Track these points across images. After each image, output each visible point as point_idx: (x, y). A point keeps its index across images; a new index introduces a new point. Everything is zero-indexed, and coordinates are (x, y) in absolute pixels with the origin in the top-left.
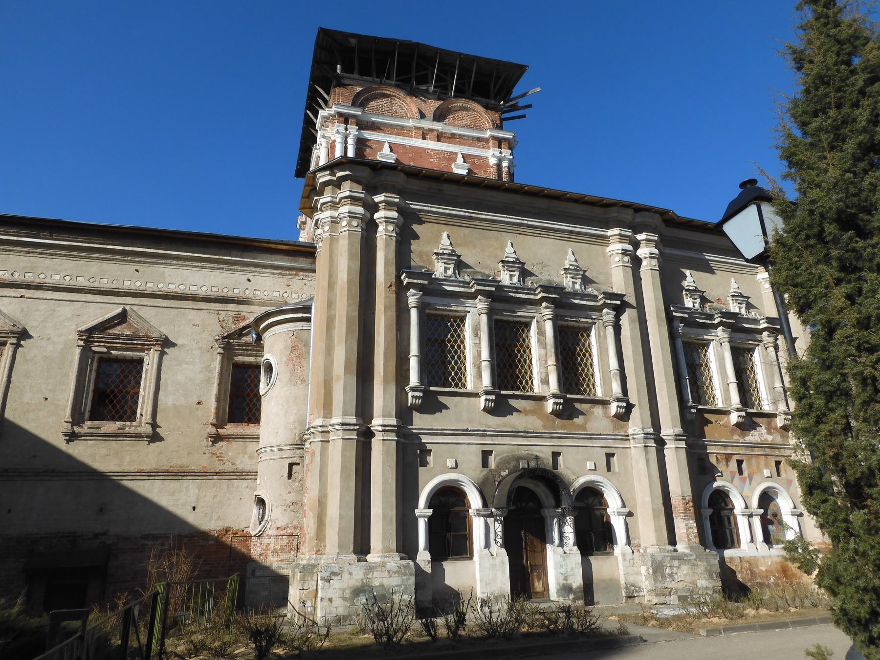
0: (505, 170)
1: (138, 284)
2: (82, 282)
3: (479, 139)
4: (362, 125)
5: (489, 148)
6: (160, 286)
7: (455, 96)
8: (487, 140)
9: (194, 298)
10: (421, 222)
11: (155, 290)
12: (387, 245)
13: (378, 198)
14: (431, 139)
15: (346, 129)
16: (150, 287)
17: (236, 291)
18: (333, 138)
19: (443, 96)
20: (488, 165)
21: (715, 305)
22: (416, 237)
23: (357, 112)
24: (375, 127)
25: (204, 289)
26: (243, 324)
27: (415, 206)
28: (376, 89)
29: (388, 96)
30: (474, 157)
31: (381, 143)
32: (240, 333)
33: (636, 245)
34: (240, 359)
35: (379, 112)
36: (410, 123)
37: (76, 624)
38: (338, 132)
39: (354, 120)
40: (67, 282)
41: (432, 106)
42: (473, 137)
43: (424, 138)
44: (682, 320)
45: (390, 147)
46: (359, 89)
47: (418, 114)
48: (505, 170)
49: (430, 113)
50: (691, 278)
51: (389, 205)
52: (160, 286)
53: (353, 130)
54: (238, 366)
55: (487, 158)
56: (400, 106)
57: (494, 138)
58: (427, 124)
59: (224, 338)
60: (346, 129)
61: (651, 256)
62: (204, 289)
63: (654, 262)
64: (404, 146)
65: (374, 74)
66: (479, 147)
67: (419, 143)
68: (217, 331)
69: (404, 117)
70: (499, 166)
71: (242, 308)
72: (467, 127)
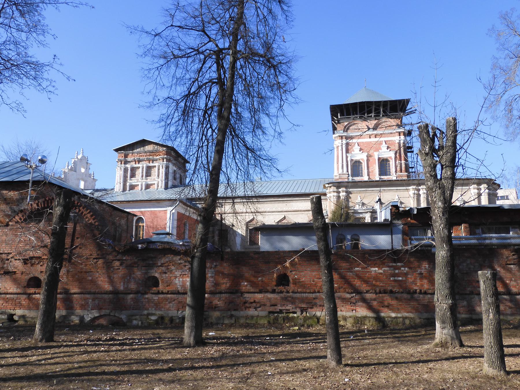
2: (274, 210)
3: (391, 133)
4: (347, 138)
7: (383, 116)
10: (351, 193)
13: (340, 190)
16: (290, 209)
19: (377, 118)
20: (395, 143)
22: (350, 198)
23: (345, 134)
24: (352, 138)
27: (351, 190)
30: (390, 141)
37: (143, 271)
40: (271, 210)
41: (372, 123)
43: (370, 138)
46: (346, 123)
53: (344, 141)
58: (370, 132)
64: (363, 143)
66: (391, 136)
70: (399, 144)
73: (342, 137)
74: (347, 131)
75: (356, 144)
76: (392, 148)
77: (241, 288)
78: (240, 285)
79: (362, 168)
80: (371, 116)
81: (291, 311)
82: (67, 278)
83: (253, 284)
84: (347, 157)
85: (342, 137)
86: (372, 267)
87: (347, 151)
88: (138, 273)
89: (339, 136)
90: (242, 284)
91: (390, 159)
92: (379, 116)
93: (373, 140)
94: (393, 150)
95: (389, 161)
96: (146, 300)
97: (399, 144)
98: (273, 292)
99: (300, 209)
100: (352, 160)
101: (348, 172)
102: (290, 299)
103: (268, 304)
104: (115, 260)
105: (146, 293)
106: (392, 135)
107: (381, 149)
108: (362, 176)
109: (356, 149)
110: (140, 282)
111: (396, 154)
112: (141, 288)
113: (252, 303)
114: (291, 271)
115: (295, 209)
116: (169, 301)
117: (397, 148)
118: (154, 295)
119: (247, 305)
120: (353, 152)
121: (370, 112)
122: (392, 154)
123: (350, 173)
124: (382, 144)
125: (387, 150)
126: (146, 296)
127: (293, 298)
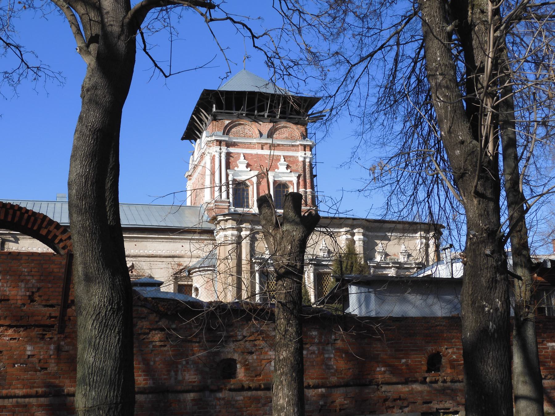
0: (307, 164)
1: (137, 251)
3: (293, 146)
5: (298, 151)
6: (146, 251)
8: (298, 146)
9: (160, 257)
11: (144, 254)
12: (246, 246)
14: (266, 149)
15: (220, 149)
16: (142, 252)
17: (177, 252)
18: (213, 154)
20: (298, 161)
21: (392, 257)
23: (270, 141)
24: (234, 145)
25: (164, 252)
26: (181, 268)
28: (236, 121)
29: (242, 124)
30: (290, 157)
31: (239, 154)
32: (181, 271)
33: (353, 235)
34: (179, 283)
35: (238, 135)
36: (255, 141)
38: (216, 151)
39: (224, 143)
41: (266, 127)
42: (290, 145)
43: (262, 149)
44: (373, 267)
45: (244, 156)
46: (227, 122)
47: (259, 135)
48: (307, 164)
49: (265, 133)
50: (380, 246)
51: (247, 229)
52: (146, 251)
53: (224, 149)
54: (180, 286)
55: (297, 157)
56: (249, 130)
57: (301, 145)
59: (174, 274)
60: (220, 149)
61: (360, 240)
62: (164, 252)
63: (361, 242)
64: (251, 155)
65: (234, 108)
66: (293, 151)
67: (260, 152)
68: (171, 272)
69: (250, 137)
70: (304, 162)
71: (180, 259)
72: (287, 138)
73: (220, 142)
74: (227, 134)
75: (242, 155)
76: (293, 168)
77: (376, 376)
78: (375, 371)
79: (248, 194)
80: (263, 116)
81: (451, 410)
82: (58, 364)
83: (393, 370)
84: (227, 175)
85: (220, 142)
86: (548, 342)
87: (228, 167)
88: (199, 353)
89: (217, 141)
90: (378, 369)
91: (290, 185)
92: (275, 117)
93: (266, 152)
94: (296, 171)
95: (247, 186)
96: (222, 402)
97: (304, 162)
98: (424, 382)
99: (159, 253)
100: (234, 180)
101: (228, 198)
102: (449, 391)
103: (420, 401)
104: (155, 329)
105: (220, 390)
106: (294, 148)
107: (278, 168)
108: (248, 207)
109: (241, 166)
110: (207, 369)
111: (299, 177)
112: (209, 381)
113: (395, 400)
114: (446, 349)
115: (151, 252)
116: (263, 401)
117: (301, 171)
118: (234, 393)
119: (388, 403)
120: (236, 169)
121: (261, 109)
122: (293, 178)
123: (231, 200)
124: (279, 160)
125: (246, 169)
126: (220, 395)
127: (452, 390)
